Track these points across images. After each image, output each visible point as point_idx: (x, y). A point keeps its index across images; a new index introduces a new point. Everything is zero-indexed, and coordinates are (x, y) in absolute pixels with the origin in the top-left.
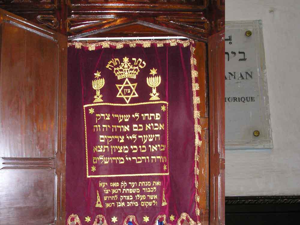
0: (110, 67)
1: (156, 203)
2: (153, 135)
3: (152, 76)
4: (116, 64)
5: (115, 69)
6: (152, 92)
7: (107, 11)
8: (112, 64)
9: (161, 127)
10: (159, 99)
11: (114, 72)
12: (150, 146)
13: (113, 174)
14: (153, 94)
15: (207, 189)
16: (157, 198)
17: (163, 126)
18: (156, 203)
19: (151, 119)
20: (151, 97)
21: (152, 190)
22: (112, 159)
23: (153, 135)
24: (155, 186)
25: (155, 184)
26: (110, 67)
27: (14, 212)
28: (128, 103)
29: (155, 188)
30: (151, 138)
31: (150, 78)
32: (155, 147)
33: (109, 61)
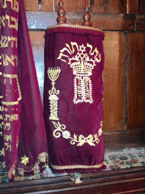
0: (63, 57)
1: (9, 148)
4: (92, 54)
5: (70, 60)
7: (56, 191)
8: (65, 53)
11: (70, 63)
13: (72, 164)
18: (9, 148)
24: (8, 121)
25: (8, 118)
26: (63, 57)
27: (72, 122)
28: (95, 61)
29: (8, 124)
32: (11, 58)
33: (62, 49)
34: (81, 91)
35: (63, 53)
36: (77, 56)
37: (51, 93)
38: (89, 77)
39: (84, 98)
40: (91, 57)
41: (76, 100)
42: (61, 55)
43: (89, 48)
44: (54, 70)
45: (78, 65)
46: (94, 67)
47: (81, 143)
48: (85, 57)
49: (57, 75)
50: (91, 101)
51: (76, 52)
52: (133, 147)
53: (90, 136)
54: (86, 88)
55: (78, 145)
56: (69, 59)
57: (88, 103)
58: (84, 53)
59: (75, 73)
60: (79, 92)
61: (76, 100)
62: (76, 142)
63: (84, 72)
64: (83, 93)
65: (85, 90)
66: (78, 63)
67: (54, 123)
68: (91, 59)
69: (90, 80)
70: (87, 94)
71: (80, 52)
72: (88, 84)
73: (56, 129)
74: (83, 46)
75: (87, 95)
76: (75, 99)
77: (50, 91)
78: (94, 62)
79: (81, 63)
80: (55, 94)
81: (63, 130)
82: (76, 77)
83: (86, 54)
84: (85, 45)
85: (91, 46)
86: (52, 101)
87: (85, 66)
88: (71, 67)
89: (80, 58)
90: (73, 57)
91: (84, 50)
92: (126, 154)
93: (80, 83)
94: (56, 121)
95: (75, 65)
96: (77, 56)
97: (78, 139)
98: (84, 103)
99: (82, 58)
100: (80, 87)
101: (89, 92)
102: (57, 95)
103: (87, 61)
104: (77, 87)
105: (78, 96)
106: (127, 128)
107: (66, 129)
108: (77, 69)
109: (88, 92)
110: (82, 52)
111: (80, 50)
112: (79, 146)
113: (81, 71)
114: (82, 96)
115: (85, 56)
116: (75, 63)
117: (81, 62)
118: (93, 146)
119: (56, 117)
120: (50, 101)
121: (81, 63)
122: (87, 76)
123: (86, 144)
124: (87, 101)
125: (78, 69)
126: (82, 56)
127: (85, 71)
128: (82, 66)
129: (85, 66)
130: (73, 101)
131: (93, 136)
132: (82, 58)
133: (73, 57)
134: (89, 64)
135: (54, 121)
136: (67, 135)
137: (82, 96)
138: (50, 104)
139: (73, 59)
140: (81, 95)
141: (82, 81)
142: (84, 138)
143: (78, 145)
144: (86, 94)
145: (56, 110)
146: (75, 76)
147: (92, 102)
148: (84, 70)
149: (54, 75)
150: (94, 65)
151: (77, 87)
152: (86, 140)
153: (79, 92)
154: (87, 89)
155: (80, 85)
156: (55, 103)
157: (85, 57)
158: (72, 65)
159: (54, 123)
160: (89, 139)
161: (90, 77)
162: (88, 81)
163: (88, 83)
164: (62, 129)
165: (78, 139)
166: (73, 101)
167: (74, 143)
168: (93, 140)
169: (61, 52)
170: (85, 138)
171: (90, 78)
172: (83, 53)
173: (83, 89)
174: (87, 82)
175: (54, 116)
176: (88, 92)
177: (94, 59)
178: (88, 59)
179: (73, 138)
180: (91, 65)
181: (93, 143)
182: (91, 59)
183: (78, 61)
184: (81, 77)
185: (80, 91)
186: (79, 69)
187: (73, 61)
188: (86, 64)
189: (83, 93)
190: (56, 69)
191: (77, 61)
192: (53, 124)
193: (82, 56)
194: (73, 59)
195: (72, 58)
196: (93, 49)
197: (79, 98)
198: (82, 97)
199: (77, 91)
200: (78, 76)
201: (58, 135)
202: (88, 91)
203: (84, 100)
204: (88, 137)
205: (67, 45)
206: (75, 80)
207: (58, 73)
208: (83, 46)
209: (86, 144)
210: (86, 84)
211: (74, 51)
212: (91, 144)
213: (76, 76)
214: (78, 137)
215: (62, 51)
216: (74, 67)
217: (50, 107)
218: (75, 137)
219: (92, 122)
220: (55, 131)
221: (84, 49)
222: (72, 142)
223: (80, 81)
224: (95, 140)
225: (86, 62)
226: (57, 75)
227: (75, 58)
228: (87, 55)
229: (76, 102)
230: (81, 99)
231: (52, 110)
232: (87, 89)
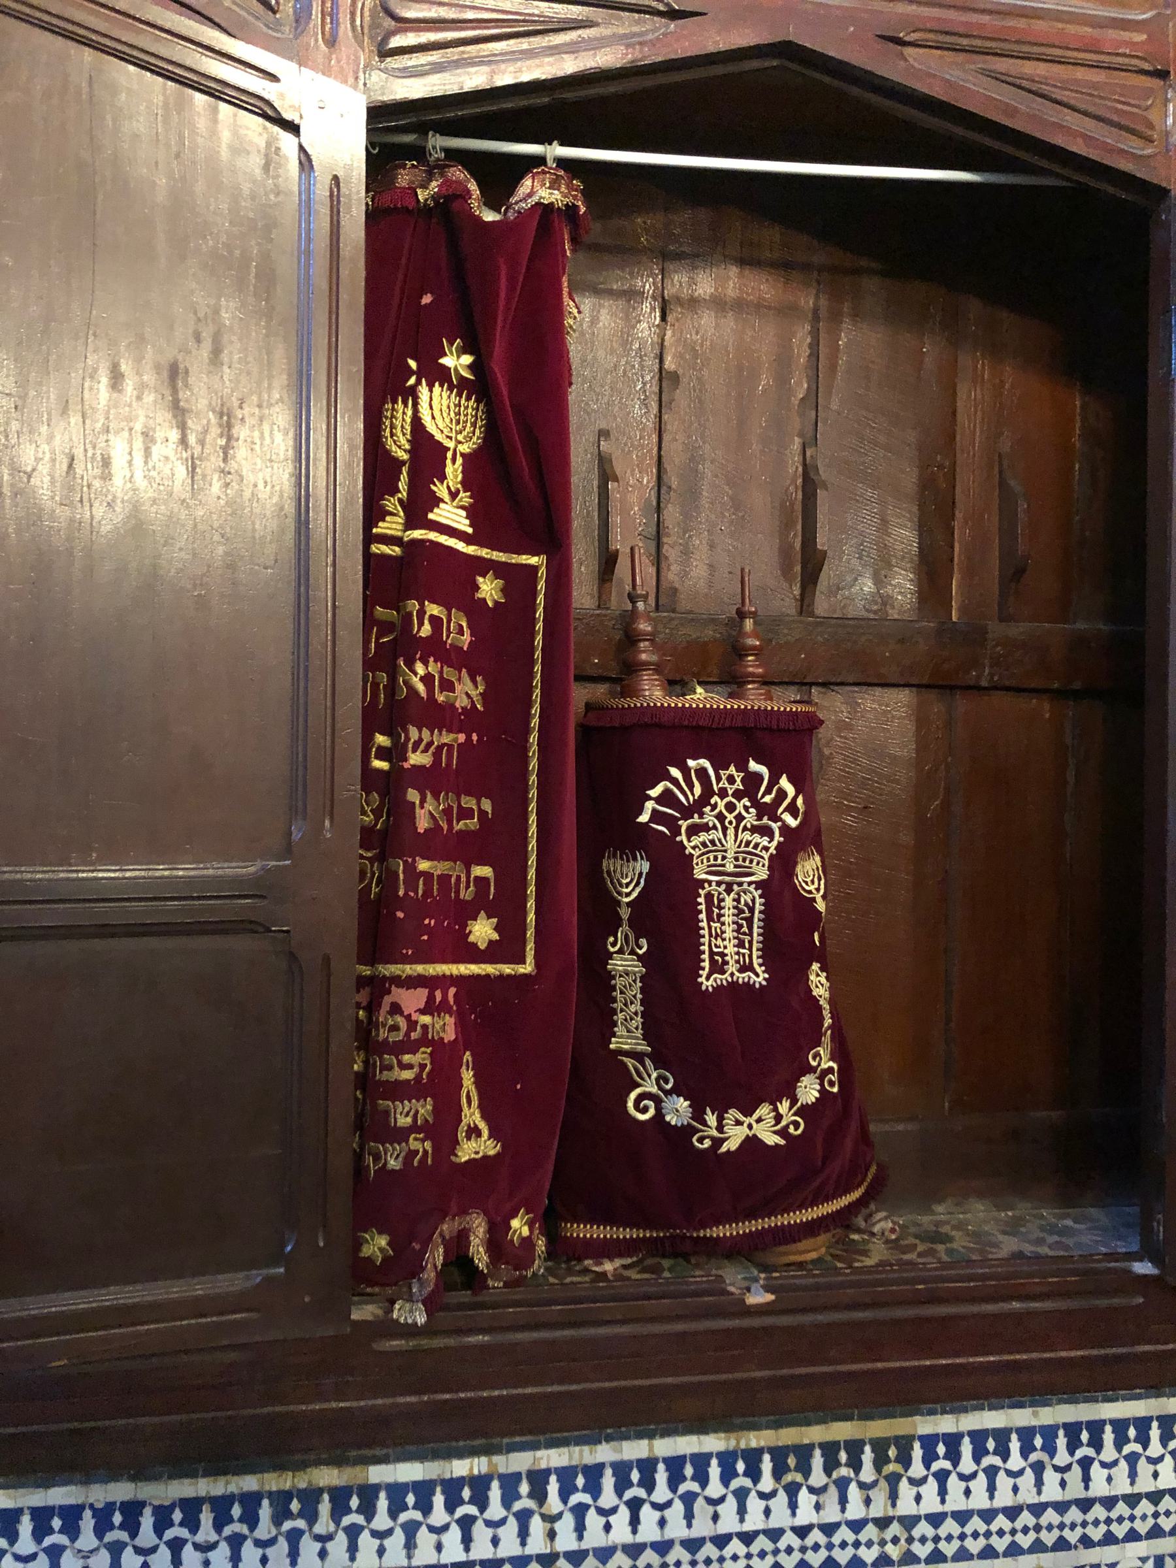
1: (425, 1152)
2: (420, 732)
3: (441, 376)
5: (684, 825)
6: (443, 478)
8: (667, 798)
9: (467, 692)
10: (470, 530)
12: (413, 795)
14: (448, 487)
15: (667, 26)
16: (430, 1119)
17: (481, 689)
19: (426, 630)
20: (437, 501)
21: (410, 1067)
22: (459, 805)
23: (420, 732)
26: (656, 816)
28: (779, 824)
30: (422, 747)
31: (437, 388)
34: (724, 940)
35: (658, 800)
36: (709, 808)
37: (616, 948)
38: (756, 889)
39: (732, 968)
40: (764, 810)
41: (708, 979)
42: (650, 805)
43: (759, 777)
44: (628, 861)
45: (713, 842)
46: (776, 849)
47: (735, 1138)
48: (740, 813)
49: (638, 884)
50: (760, 978)
51: (708, 792)
52: (981, 1195)
53: (764, 1110)
54: (741, 926)
55: (724, 1149)
56: (680, 822)
57: (748, 986)
58: (738, 795)
59: (699, 873)
60: (716, 946)
61: (708, 979)
62: (713, 1138)
63: (736, 866)
64: (730, 951)
65: (735, 934)
66: (716, 835)
67: (630, 1062)
68: (766, 818)
69: (760, 897)
70: (742, 951)
71: (723, 793)
72: (747, 914)
73: (639, 1085)
74: (732, 770)
75: (744, 955)
76: (704, 973)
77: (611, 939)
78: (775, 826)
79: (725, 835)
80: (633, 953)
81: (667, 1093)
82: (703, 888)
83: (746, 801)
84: (742, 767)
85: (763, 770)
86: (621, 976)
87: (739, 846)
88: (689, 850)
89: (721, 817)
90: (696, 816)
91: (739, 785)
92: (947, 1223)
93: (720, 908)
94: (638, 1056)
95: (704, 844)
96: (709, 808)
97: (720, 1128)
98: (733, 985)
99: (730, 817)
100: (718, 925)
101: (751, 942)
102: (640, 958)
103: (749, 826)
104: (710, 928)
105: (713, 962)
106: (950, 1109)
107: (676, 1091)
108: (711, 856)
109: (747, 945)
110: (730, 792)
111: (724, 783)
112: (728, 1151)
113: (723, 866)
114: (727, 958)
115: (740, 807)
116: (704, 837)
117: (725, 829)
118: (777, 1145)
119: (637, 1038)
120: (614, 978)
121: (725, 835)
122: (750, 884)
123: (751, 1143)
124: (742, 977)
125: (720, 857)
126: (731, 807)
127: (740, 862)
128: (730, 843)
129: (739, 846)
130: (700, 980)
131: (776, 1109)
132: (730, 817)
133: (696, 816)
134: (757, 838)
135: (628, 1054)
136: (678, 1110)
137: (727, 958)
138: (614, 988)
139: (696, 819)
140: (723, 955)
141: (729, 901)
142: (741, 1118)
143: (724, 1149)
144: (738, 953)
145: (636, 1013)
146: (701, 883)
147: (765, 979)
148: (736, 859)
149: (628, 880)
150: (777, 838)
151: (710, 928)
152: (750, 1127)
153: (716, 946)
154: (744, 934)
155: (720, 916)
156: (630, 985)
157: (740, 813)
158: (691, 845)
159: (630, 1062)
160: (759, 1120)
161: (759, 885)
162: (753, 901)
163: (752, 910)
164: (660, 1088)
165: (720, 1128)
166: (700, 980)
167: (707, 1143)
168: (773, 1123)
169: (649, 798)
170: (747, 1120)
171: (760, 892)
172: (733, 795)
173: (729, 933)
174: (746, 904)
175: (627, 1037)
176: (747, 945)
177: (776, 818)
178: (750, 819)
179: (705, 1124)
180: (764, 841)
181: (775, 1132)
182: (766, 818)
183: (715, 827)
184: (723, 887)
185: (719, 942)
186: (716, 858)
187: (693, 831)
188: (747, 836)
189: (730, 951)
190: (635, 859)
191: (711, 824)
192: (625, 1065)
193: (731, 807)
194: (696, 819)
195: (680, 827)
196: (774, 781)
197: (718, 967)
198: (727, 963)
199: (710, 941)
200: (714, 884)
201: (645, 1110)
202: (747, 938)
203: (732, 974)
204: (755, 1116)
205: (675, 772)
206: (701, 900)
207: (641, 874)
208: (732, 770)
209: (751, 1143)
210: (741, 911)
211: (698, 790)
212: (771, 1139)
213: (706, 885)
214: (720, 1119)
215: (655, 792)
216: (696, 853)
217: (614, 1000)
218: (711, 1119)
219: (945, 1239)
220: (633, 1096)
221: (738, 780)
222: (701, 1140)
223: (721, 900)
224: (784, 1123)
225: (745, 829)
226: (638, 884)
227: (701, 816)
228: (748, 804)
229: (707, 983)
230: (723, 972)
231: (622, 1011)
232: (744, 934)
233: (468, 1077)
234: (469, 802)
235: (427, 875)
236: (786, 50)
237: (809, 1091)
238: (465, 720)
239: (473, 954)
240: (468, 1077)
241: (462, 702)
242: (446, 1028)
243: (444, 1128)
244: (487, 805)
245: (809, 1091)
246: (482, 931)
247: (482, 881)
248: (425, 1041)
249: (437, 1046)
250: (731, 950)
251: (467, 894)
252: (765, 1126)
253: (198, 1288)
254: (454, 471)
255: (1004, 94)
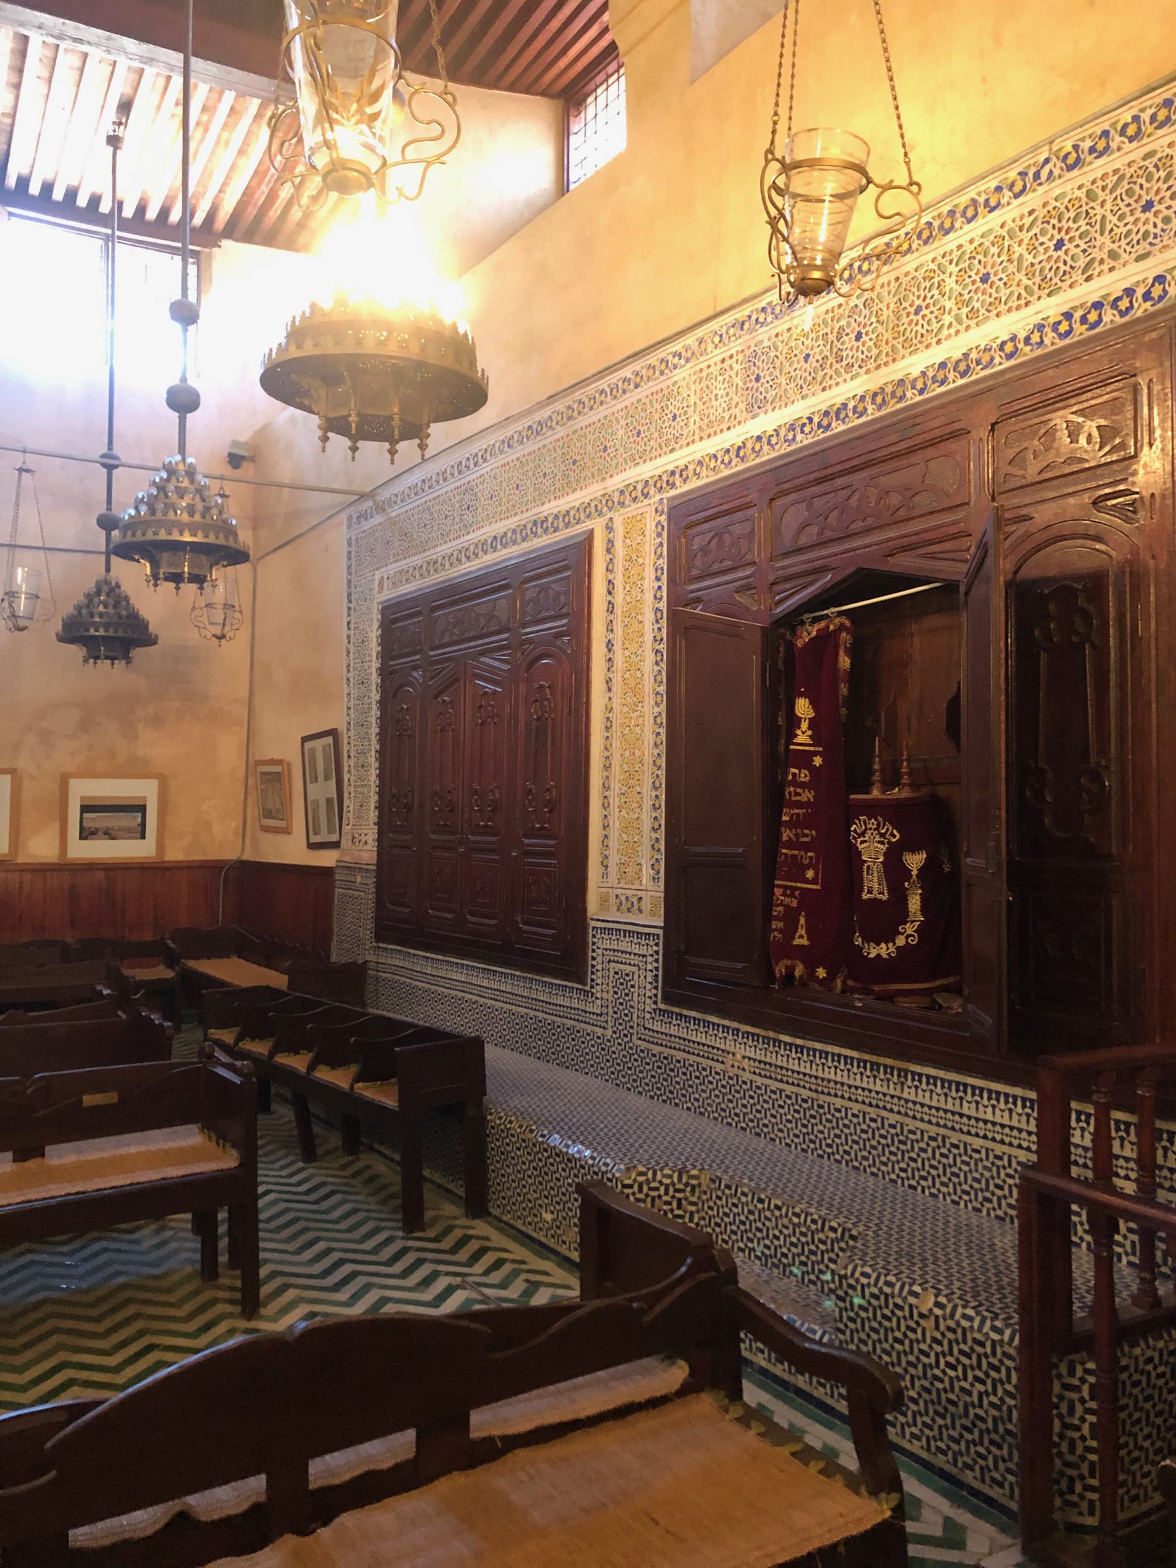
6: (799, 728)
19: (790, 777)
20: (796, 735)
53: (883, 945)
57: (880, 900)
98: (875, 899)
123: (879, 955)
158: (860, 847)
173: (876, 880)
187: (862, 842)
209: (879, 955)
212: (885, 956)
229: (865, 896)
233: (802, 921)
234: (807, 831)
235: (786, 854)
236: (860, 570)
237: (901, 941)
238: (807, 805)
239: (807, 881)
240: (802, 921)
241: (805, 799)
242: (795, 904)
243: (790, 930)
244: (814, 833)
245: (901, 941)
246: (810, 874)
247: (811, 858)
248: (781, 904)
249: (787, 907)
250: (876, 886)
251: (806, 862)
252: (884, 950)
253: (720, 964)
254: (804, 725)
255: (918, 560)
